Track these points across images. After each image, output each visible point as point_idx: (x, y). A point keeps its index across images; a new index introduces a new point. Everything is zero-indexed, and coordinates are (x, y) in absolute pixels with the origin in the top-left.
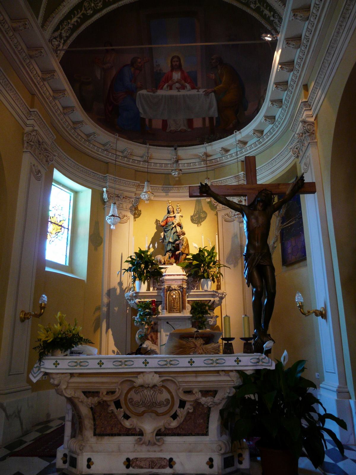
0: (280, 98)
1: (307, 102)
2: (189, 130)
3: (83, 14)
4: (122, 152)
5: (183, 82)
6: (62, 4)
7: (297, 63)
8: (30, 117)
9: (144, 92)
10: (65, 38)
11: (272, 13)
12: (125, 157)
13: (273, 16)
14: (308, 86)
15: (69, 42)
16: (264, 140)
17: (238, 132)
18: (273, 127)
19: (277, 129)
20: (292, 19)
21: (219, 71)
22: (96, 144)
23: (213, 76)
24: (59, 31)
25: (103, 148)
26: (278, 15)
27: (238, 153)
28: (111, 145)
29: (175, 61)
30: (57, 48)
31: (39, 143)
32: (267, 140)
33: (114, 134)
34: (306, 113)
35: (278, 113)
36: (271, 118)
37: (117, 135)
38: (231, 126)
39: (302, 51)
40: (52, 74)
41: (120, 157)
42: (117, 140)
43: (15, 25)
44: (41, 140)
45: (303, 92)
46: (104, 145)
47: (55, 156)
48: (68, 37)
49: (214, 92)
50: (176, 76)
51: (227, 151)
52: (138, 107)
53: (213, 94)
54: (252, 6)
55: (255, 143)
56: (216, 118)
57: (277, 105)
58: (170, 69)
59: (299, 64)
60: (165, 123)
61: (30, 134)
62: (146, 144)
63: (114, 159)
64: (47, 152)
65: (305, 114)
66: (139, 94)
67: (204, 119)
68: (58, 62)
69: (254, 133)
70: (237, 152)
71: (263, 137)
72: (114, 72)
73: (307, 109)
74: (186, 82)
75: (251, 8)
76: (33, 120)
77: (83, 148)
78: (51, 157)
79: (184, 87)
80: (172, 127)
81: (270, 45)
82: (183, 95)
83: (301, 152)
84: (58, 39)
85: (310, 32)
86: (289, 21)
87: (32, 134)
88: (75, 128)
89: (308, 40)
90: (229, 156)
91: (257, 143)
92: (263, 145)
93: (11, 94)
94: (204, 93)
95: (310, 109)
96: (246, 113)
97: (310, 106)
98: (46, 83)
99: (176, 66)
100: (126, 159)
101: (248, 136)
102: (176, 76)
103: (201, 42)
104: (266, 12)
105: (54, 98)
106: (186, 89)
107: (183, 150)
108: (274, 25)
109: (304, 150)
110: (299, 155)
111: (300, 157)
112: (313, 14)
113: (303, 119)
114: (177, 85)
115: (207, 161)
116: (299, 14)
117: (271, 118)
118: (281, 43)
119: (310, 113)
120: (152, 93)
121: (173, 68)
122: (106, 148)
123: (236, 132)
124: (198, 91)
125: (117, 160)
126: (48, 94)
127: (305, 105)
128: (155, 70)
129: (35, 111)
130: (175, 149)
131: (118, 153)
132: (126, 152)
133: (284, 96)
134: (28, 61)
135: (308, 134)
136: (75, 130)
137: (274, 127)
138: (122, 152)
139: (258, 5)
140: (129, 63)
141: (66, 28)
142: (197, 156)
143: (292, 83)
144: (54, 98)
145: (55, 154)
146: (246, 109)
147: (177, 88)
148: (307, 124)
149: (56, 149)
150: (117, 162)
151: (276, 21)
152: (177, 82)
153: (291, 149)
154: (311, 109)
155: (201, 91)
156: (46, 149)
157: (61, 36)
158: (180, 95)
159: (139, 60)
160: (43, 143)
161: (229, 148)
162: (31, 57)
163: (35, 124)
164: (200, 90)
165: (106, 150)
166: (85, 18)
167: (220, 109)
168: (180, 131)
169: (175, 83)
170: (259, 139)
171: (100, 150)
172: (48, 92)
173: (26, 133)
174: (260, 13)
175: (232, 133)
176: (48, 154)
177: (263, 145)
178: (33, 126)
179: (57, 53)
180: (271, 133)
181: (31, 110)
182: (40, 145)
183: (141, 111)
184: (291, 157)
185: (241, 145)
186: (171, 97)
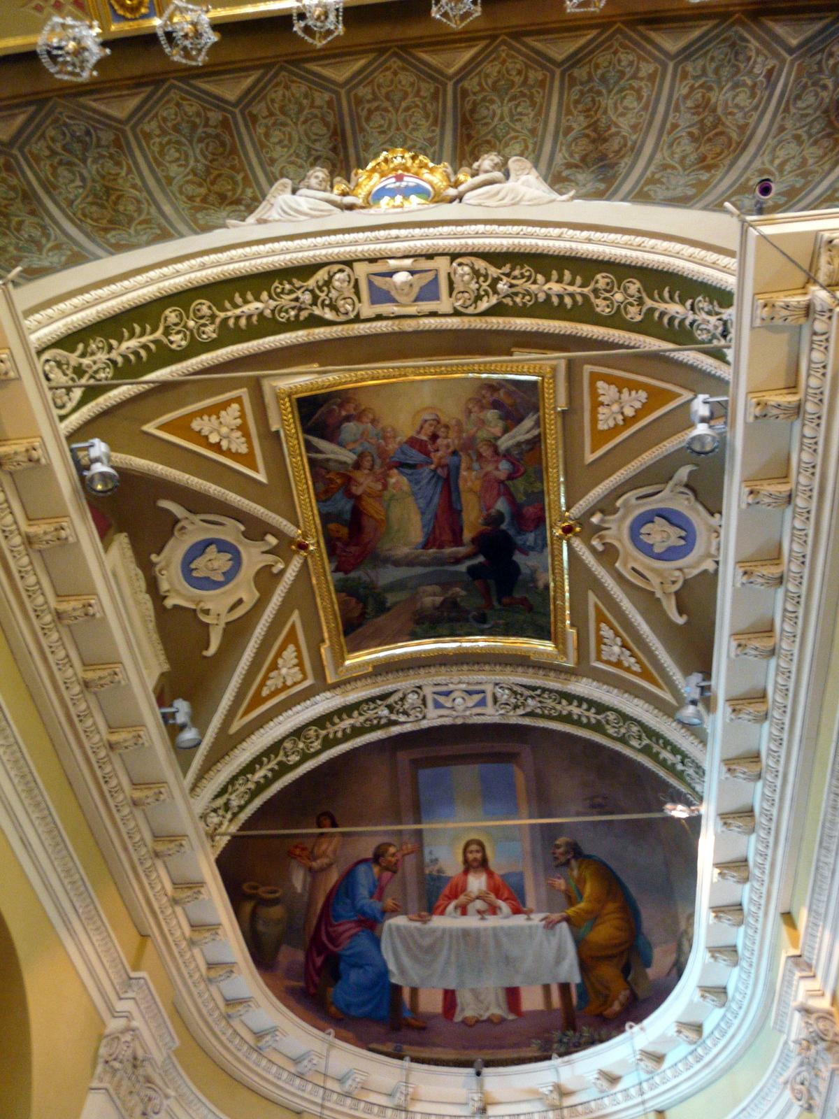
0: (730, 942)
1: (800, 956)
2: (511, 1017)
3: (280, 763)
4: (341, 1081)
5: (492, 896)
6: (239, 747)
7: (768, 755)
8: (126, 992)
9: (400, 921)
10: (236, 810)
11: (679, 757)
12: (347, 1095)
13: (682, 762)
14: (794, 915)
15: (244, 816)
16: (707, 1050)
17: (636, 1028)
18: (724, 1016)
19: (736, 1022)
20: (727, 778)
21: (575, 873)
22: (276, 1058)
23: (561, 883)
24: (226, 797)
25: (293, 1070)
26: (693, 761)
27: (645, 1086)
28: (314, 1062)
29: (471, 852)
30: (216, 829)
31: (135, 1062)
32: (718, 1051)
33: (322, 1030)
34: (805, 986)
35: (732, 978)
36: (718, 993)
37: (329, 1034)
38: (616, 1007)
39: (759, 839)
40: (196, 890)
41: (335, 1097)
42: (332, 1046)
43: (137, 795)
44: (140, 1054)
45: (784, 931)
46: (296, 1061)
47: (167, 1097)
48: (241, 808)
49: (568, 920)
50: (477, 883)
51: (613, 1080)
52: (385, 957)
53: (564, 925)
54: (634, 743)
55: (686, 1058)
56: (578, 986)
57: (739, 827)
58: (461, 868)
59: (761, 867)
60: (450, 998)
61: (118, 1038)
62: (401, 1058)
63: (319, 1100)
64: (149, 1088)
65: (802, 991)
66: (390, 925)
67: (547, 988)
68: (213, 858)
69: (679, 1032)
70: (640, 1084)
71: (704, 1042)
72: (334, 877)
73: (805, 974)
74: (498, 896)
75: (632, 747)
76: (132, 1001)
77: (245, 1071)
78: (157, 1102)
79: (494, 910)
80: (468, 1009)
81: (686, 826)
82: (494, 929)
83: (815, 1094)
84: (221, 812)
85: (806, 515)
86: (720, 782)
87: (123, 1040)
88: (229, 1016)
89: (804, 538)
90: (619, 1096)
91: (691, 1059)
92: (707, 1065)
93: (94, 939)
94: (544, 922)
95: (812, 974)
96: (652, 972)
97: (809, 966)
98: (179, 910)
99: (476, 862)
100: (349, 1101)
101: (664, 1039)
102: (477, 883)
103: (531, 817)
104: (665, 754)
105: (192, 943)
106: (498, 912)
107: (500, 1075)
108: (688, 778)
109: (823, 1087)
110: (811, 1102)
111: (815, 1109)
112: (788, 614)
113: (802, 1003)
114: (479, 904)
115: (561, 1108)
116: (740, 769)
117: (718, 993)
118: (711, 823)
119: (816, 985)
120: (418, 924)
121: (469, 867)
122: (300, 1068)
123: (631, 1027)
124: (529, 919)
125: (327, 1104)
126: (178, 934)
127: (797, 964)
128: (427, 872)
129: (140, 978)
130: (478, 1074)
131: (331, 1085)
132: (350, 1082)
133: (739, 937)
134: (148, 863)
135: (822, 1045)
136: (228, 1023)
137: (729, 1015)
138: (339, 1080)
139: (646, 741)
140: (370, 855)
141: (242, 789)
142: (536, 1096)
143: (753, 909)
144: (192, 943)
145: (172, 1093)
146: (648, 963)
147: (479, 912)
148: (815, 1015)
149: (174, 1074)
150: (326, 1112)
151: (691, 771)
152: (478, 898)
153: (786, 1083)
154: (814, 976)
155: (537, 919)
156: (148, 1080)
157: (227, 806)
158: (486, 929)
159: (392, 850)
160: (143, 1061)
161: (617, 1072)
162: (157, 855)
163: (136, 1013)
164: (532, 916)
165: (300, 1076)
166: (284, 768)
167: (585, 965)
168: (489, 1020)
169: (472, 900)
170: (693, 1047)
171: (285, 1075)
172: (181, 927)
173: (107, 1036)
174: (655, 757)
175: (621, 1030)
176: (150, 1093)
177: (707, 1065)
178: (129, 1017)
179: (213, 841)
180: (724, 1033)
181: (133, 975)
182: (135, 1066)
183: (392, 966)
184: (789, 1107)
185: (650, 1064)
186: (465, 933)
